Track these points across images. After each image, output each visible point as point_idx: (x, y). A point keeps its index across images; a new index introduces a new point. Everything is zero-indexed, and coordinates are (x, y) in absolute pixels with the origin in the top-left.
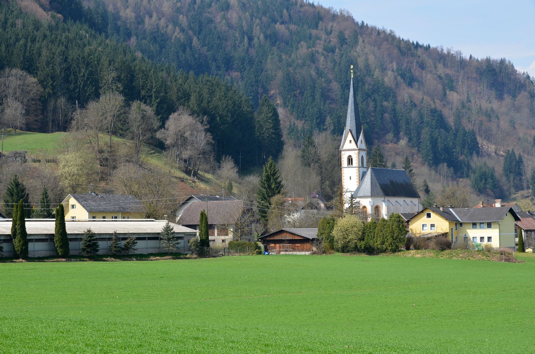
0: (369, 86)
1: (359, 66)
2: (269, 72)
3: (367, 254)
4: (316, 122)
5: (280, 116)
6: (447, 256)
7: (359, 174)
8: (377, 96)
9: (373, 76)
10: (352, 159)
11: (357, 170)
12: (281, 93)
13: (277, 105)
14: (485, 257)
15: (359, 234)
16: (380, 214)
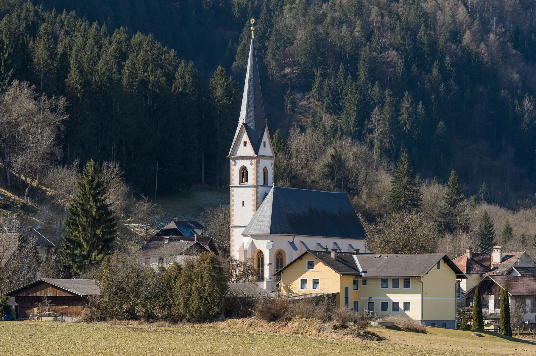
10: (247, 172)
11: (253, 190)
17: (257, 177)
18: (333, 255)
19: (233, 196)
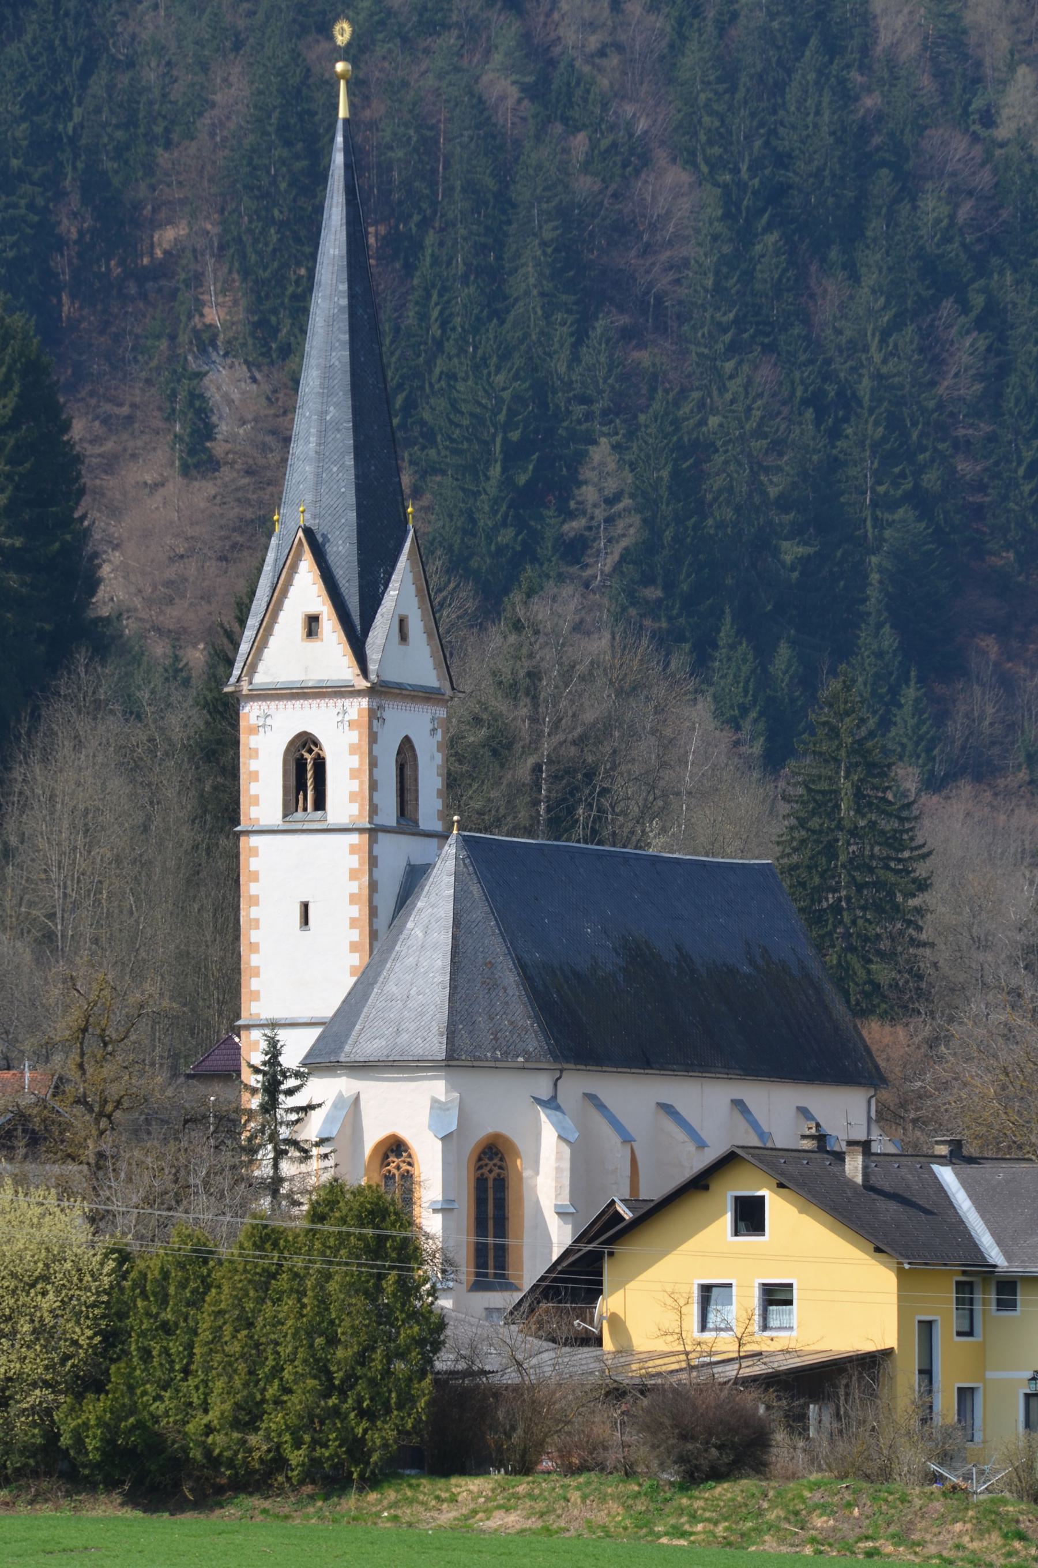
0: (957, 206)
1: (885, 39)
2: (150, 76)
3: (132, 1500)
4: (507, 482)
5: (224, 428)
6: (720, 1528)
7: (373, 887)
8: (1018, 282)
9: (988, 119)
10: (320, 765)
11: (353, 849)
12: (239, 240)
13: (205, 336)
14: (995, 1538)
15: (75, 1343)
16: (520, 1200)
17: (373, 786)
18: (854, 1167)
19: (255, 877)
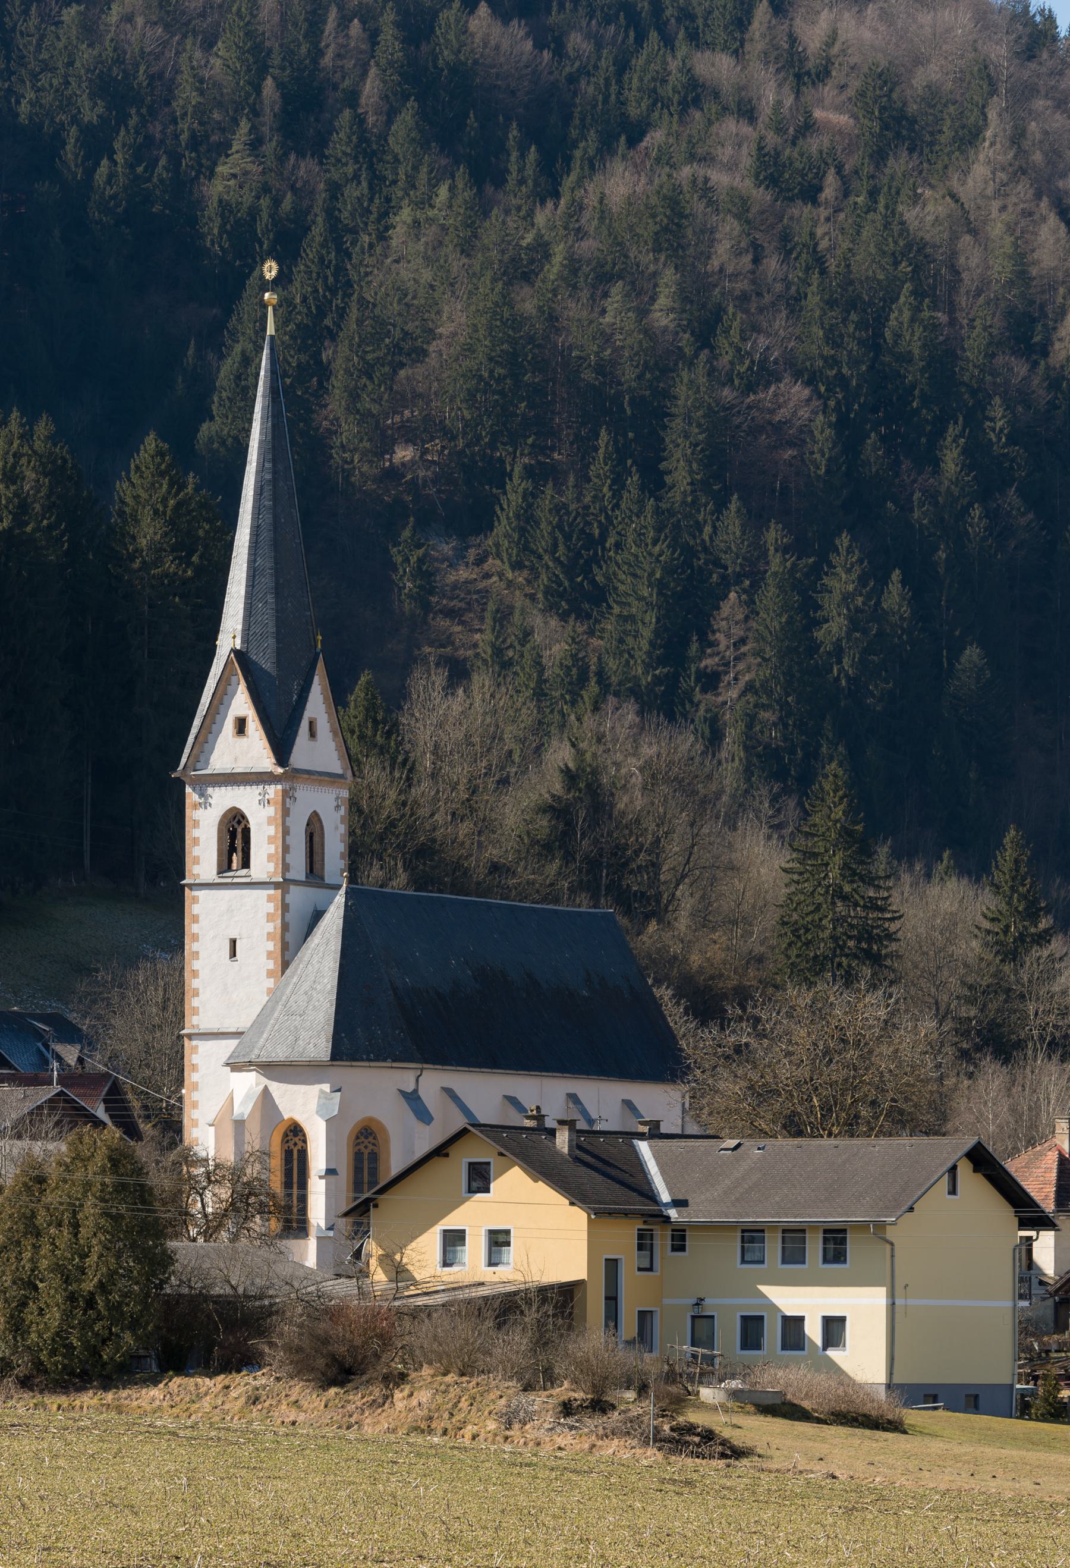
10: (247, 832)
11: (270, 899)
17: (286, 849)
18: (563, 1140)
